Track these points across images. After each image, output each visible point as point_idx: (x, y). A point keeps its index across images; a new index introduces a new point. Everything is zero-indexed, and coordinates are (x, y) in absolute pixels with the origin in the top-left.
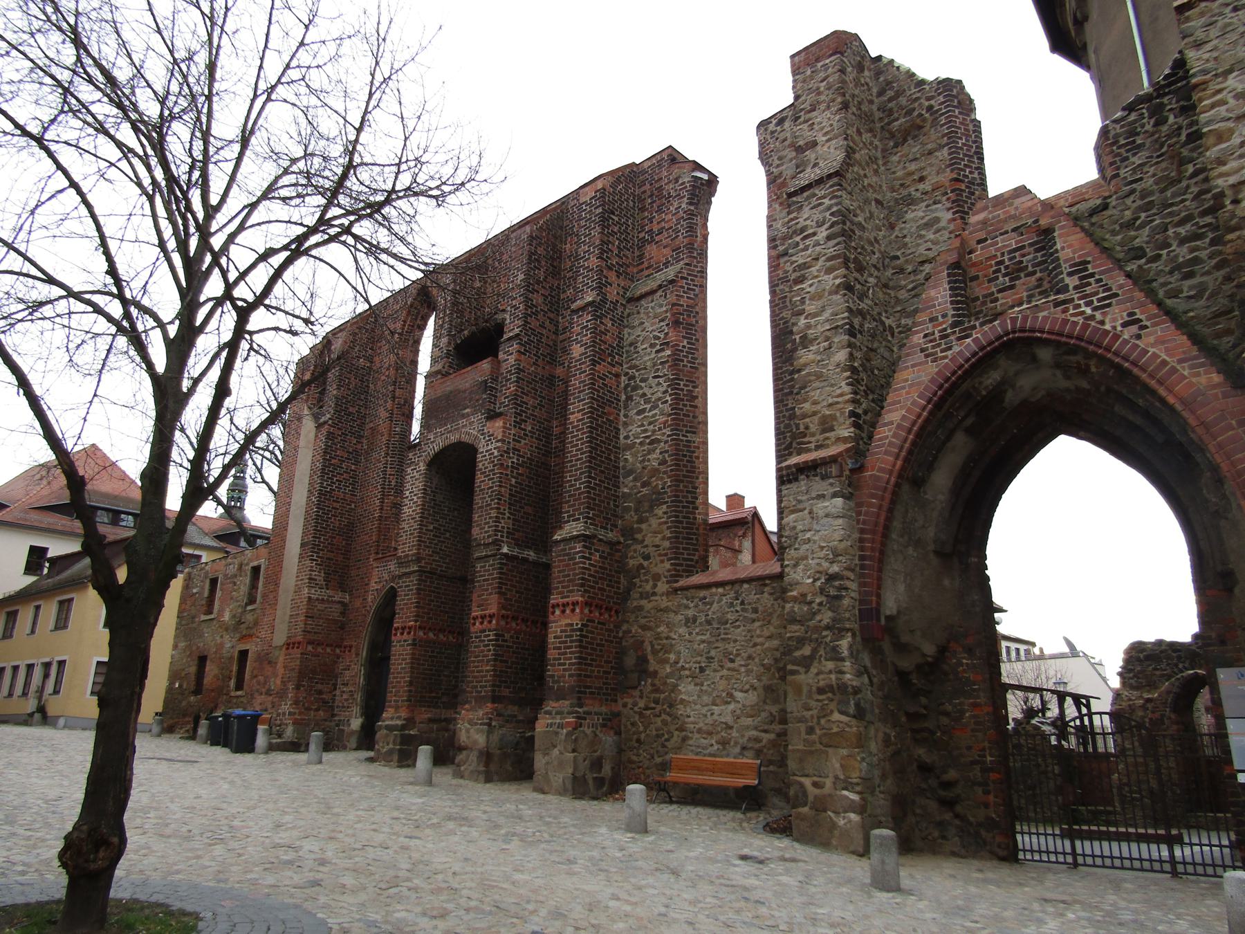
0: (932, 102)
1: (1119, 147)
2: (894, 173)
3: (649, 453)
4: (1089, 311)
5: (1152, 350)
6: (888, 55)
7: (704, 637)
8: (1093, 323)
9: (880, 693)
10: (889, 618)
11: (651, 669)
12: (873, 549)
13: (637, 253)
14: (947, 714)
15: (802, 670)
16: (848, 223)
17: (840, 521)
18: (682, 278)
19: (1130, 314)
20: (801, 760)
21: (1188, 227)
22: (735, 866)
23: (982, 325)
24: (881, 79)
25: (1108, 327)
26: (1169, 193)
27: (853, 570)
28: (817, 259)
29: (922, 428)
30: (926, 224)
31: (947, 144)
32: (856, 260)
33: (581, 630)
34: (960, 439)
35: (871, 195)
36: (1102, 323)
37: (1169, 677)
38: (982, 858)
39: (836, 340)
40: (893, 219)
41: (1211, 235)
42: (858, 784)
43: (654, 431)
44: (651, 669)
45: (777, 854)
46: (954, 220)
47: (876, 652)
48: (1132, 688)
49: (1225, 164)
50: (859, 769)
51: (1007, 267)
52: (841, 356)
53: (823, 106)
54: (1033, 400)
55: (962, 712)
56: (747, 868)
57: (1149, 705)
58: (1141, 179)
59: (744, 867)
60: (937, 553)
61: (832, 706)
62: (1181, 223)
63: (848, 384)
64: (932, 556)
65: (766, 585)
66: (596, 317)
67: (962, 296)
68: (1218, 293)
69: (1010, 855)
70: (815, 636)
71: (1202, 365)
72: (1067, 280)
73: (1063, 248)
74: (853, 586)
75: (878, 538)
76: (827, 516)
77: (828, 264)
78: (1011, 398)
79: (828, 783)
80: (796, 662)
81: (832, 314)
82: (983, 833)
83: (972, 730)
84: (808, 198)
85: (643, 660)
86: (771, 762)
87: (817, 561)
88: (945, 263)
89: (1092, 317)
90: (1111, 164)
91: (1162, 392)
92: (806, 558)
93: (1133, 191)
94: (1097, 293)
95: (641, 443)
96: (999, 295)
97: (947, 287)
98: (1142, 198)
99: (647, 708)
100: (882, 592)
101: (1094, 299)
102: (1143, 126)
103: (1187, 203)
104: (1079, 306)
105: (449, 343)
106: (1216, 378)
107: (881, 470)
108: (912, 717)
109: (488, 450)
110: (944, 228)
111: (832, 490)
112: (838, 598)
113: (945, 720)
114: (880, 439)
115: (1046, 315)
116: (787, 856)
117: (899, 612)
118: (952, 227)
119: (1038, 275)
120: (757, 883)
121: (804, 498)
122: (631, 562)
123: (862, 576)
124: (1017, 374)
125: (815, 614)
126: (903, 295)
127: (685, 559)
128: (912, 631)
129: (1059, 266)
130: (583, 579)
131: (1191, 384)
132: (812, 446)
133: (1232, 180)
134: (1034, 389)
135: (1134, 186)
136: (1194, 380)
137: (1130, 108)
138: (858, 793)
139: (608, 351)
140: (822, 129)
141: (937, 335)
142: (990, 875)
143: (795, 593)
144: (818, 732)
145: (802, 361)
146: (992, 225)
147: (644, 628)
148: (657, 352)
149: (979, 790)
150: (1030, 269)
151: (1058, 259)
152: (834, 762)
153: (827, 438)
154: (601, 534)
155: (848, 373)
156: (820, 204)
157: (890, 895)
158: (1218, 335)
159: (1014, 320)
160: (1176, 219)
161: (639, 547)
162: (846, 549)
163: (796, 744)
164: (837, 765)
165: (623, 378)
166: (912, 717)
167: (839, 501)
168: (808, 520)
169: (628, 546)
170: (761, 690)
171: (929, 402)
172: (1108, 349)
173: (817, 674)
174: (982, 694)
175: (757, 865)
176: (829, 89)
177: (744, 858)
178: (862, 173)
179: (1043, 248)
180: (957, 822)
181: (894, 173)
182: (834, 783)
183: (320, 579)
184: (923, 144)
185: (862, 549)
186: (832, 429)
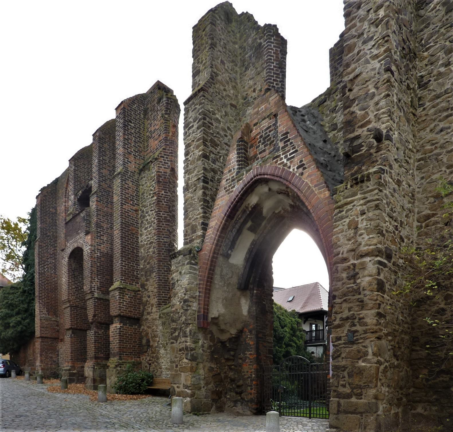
3: (149, 249)
11: (151, 344)
12: (203, 288)
13: (146, 144)
14: (241, 359)
15: (175, 342)
16: (208, 119)
18: (161, 157)
25: (291, 170)
32: (212, 141)
33: (120, 329)
35: (227, 101)
36: (289, 167)
39: (198, 186)
43: (151, 238)
63: (201, 209)
66: (122, 181)
71: (323, 187)
79: (181, 386)
83: (249, 365)
85: (148, 341)
95: (147, 244)
97: (236, 152)
99: (150, 360)
101: (288, 154)
105: (75, 198)
109: (87, 249)
114: (208, 236)
122: (144, 299)
127: (163, 297)
130: (119, 307)
139: (132, 198)
141: (231, 179)
144: (179, 366)
147: (149, 327)
148: (152, 198)
154: (129, 287)
156: (195, 109)
161: (146, 292)
165: (140, 212)
169: (143, 292)
178: (222, 88)
183: (45, 311)
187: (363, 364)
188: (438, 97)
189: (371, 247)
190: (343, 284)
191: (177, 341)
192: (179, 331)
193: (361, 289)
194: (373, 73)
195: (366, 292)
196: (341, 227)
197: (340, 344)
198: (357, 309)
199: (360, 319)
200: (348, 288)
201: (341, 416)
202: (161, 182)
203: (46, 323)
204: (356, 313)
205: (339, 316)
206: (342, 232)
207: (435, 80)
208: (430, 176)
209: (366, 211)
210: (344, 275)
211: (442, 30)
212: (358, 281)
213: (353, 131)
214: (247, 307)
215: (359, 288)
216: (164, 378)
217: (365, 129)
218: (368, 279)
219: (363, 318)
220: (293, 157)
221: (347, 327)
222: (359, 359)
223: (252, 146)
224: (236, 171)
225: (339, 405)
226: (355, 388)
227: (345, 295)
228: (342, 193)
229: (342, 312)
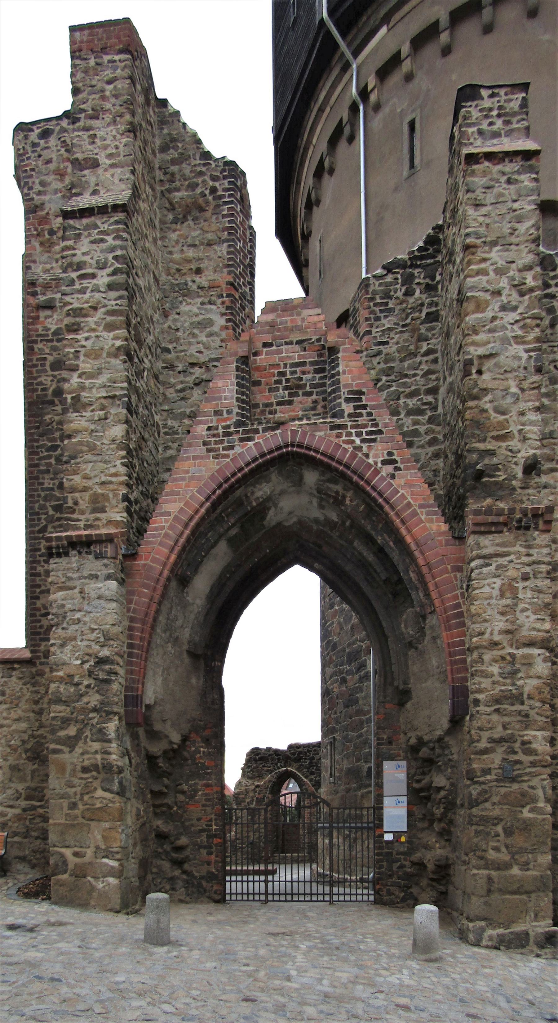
0: (217, 184)
1: (375, 305)
2: (171, 253)
4: (358, 441)
5: (401, 491)
6: (175, 104)
8: (360, 454)
9: (135, 773)
10: (148, 707)
17: (114, 605)
19: (390, 454)
20: (62, 833)
21: (415, 400)
22: (8, 938)
23: (265, 430)
24: (166, 131)
25: (371, 461)
26: (406, 364)
27: (122, 657)
28: (95, 308)
29: (198, 525)
30: (199, 323)
31: (227, 241)
34: (222, 547)
36: (367, 456)
37: (271, 771)
38: (202, 902)
40: (167, 306)
41: (429, 414)
42: (118, 853)
45: (43, 919)
46: (227, 328)
47: (135, 737)
48: (249, 778)
49: (477, 334)
50: (120, 839)
51: (287, 381)
52: (118, 431)
53: (108, 117)
54: (286, 524)
55: (196, 791)
56: (21, 940)
57: (257, 789)
58: (387, 343)
59: (16, 939)
60: (188, 652)
61: (96, 784)
62: (411, 395)
63: (123, 464)
64: (185, 655)
65: (14, 669)
67: (247, 396)
68: (427, 466)
69: (220, 899)
70: (81, 717)
71: (435, 513)
72: (344, 406)
73: (344, 372)
74: (121, 672)
75: (148, 628)
76: (99, 597)
77: (109, 318)
79: (89, 852)
80: (59, 741)
81: (110, 380)
82: (204, 883)
83: (203, 806)
84: (87, 227)
86: (16, 834)
87: (87, 643)
88: (235, 354)
89: (359, 448)
90: (367, 319)
91: (403, 531)
92: (75, 639)
93: (379, 353)
94: (366, 426)
96: (278, 408)
97: (235, 381)
98: (386, 362)
100: (145, 681)
101: (364, 430)
103: (418, 378)
104: (349, 434)
106: (444, 527)
107: (154, 560)
108: (156, 794)
110: (217, 334)
111: (106, 572)
112: (107, 682)
113: (181, 797)
114: (156, 529)
115: (322, 438)
116: (53, 920)
117: (155, 702)
118: (224, 335)
119: (314, 397)
120: (39, 955)
121: (75, 575)
123: (129, 663)
124: (282, 493)
125: (82, 695)
126: (171, 393)
128: (164, 721)
129: (338, 390)
131: (425, 529)
132: (81, 524)
133: (481, 351)
134: (290, 513)
135: (381, 347)
136: (428, 525)
137: (389, 268)
138: (118, 860)
140: (105, 147)
141: (221, 431)
142: (220, 917)
143: (61, 673)
144: (81, 807)
145: (73, 426)
146: (279, 330)
149: (204, 852)
150: (308, 388)
151: (338, 382)
152: (96, 835)
153: (97, 519)
155: (124, 453)
156: (102, 241)
157: (166, 948)
159: (294, 433)
160: (408, 391)
162: (117, 635)
163: (57, 818)
164: (99, 837)
166: (156, 794)
168: (78, 600)
170: (6, 769)
173: (82, 754)
174: (213, 777)
175: (29, 934)
176: (116, 96)
177: (12, 927)
179: (322, 370)
180: (184, 877)
181: (171, 253)
182: (95, 853)
184: (204, 232)
185: (130, 637)
186: (103, 510)
187: (531, 815)
189: (540, 634)
191: (72, 748)
193: (525, 696)
196: (487, 589)
197: (490, 781)
198: (517, 726)
199: (524, 743)
200: (501, 691)
201: (495, 897)
204: (516, 733)
205: (485, 735)
209: (531, 576)
210: (495, 669)
213: (484, 440)
215: (522, 694)
217: (504, 444)
218: (535, 682)
219: (530, 742)
225: (490, 879)
226: (517, 853)
227: (497, 701)
229: (491, 729)
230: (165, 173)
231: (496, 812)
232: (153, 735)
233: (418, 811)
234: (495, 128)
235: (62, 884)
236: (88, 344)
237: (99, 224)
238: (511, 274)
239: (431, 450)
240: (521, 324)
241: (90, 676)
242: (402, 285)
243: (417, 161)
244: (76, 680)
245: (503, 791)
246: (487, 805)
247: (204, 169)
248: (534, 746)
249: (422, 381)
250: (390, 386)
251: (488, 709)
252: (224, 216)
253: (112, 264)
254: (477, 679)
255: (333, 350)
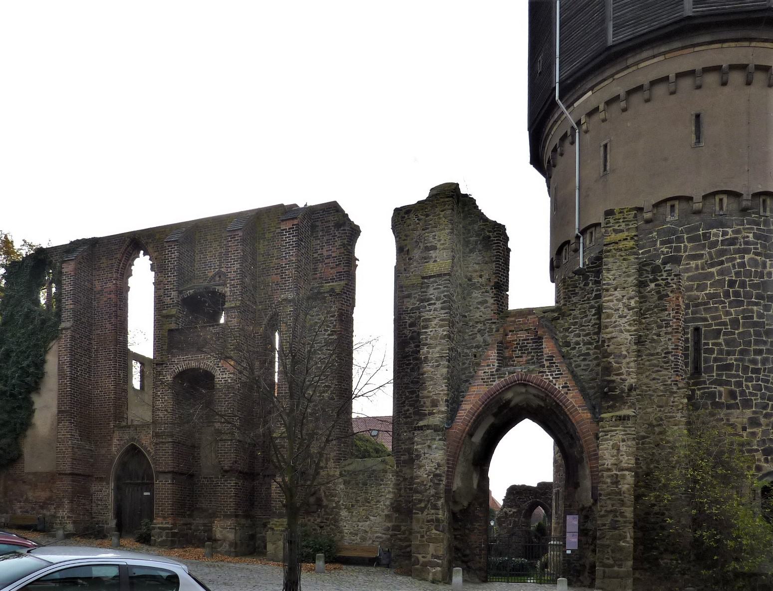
0: (491, 234)
3: (324, 392)
4: (551, 378)
7: (354, 491)
8: (552, 384)
15: (420, 513)
21: (588, 338)
25: (557, 387)
26: (584, 320)
36: (555, 385)
44: (325, 504)
46: (494, 304)
52: (445, 370)
54: (520, 405)
58: (575, 310)
62: (586, 335)
72: (545, 363)
74: (444, 479)
78: (513, 403)
87: (429, 468)
96: (516, 359)
102: (579, 284)
103: (589, 327)
107: (459, 430)
110: (489, 307)
114: (460, 416)
126: (467, 337)
129: (542, 355)
133: (609, 336)
136: (583, 415)
141: (489, 373)
150: (530, 350)
151: (542, 352)
156: (439, 288)
158: (590, 388)
167: (441, 443)
171: (483, 403)
172: (555, 396)
173: (427, 515)
179: (536, 342)
183: (77, 435)
185: (448, 463)
188: (652, 355)
190: (608, 486)
192: (426, 503)
193: (622, 492)
194: (626, 341)
195: (625, 495)
197: (606, 529)
198: (618, 505)
202: (343, 321)
203: (79, 453)
205: (605, 509)
206: (607, 449)
207: (650, 342)
208: (645, 409)
210: (609, 480)
211: (656, 310)
212: (620, 486)
213: (610, 376)
214: (477, 481)
215: (621, 491)
216: (346, 544)
217: (619, 377)
218: (627, 486)
220: (559, 378)
221: (611, 517)
222: (620, 540)
223: (507, 348)
224: (496, 367)
225: (604, 572)
227: (609, 494)
228: (608, 423)
230: (466, 230)
231: (608, 542)
232: (455, 503)
233: (583, 539)
234: (621, 228)
235: (417, 569)
236: (432, 334)
237: (437, 281)
238: (624, 301)
239: (595, 362)
240: (628, 323)
241: (431, 481)
242: (583, 281)
243: (608, 168)
244: (425, 483)
245: (611, 533)
246: (605, 540)
247: (484, 227)
248: (625, 514)
249: (592, 328)
250: (576, 331)
251: (604, 498)
252: (494, 250)
253: (443, 299)
254: (601, 485)
255: (541, 338)
